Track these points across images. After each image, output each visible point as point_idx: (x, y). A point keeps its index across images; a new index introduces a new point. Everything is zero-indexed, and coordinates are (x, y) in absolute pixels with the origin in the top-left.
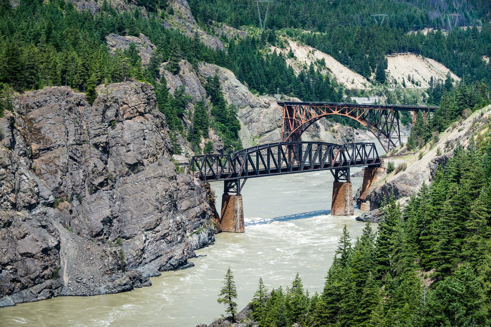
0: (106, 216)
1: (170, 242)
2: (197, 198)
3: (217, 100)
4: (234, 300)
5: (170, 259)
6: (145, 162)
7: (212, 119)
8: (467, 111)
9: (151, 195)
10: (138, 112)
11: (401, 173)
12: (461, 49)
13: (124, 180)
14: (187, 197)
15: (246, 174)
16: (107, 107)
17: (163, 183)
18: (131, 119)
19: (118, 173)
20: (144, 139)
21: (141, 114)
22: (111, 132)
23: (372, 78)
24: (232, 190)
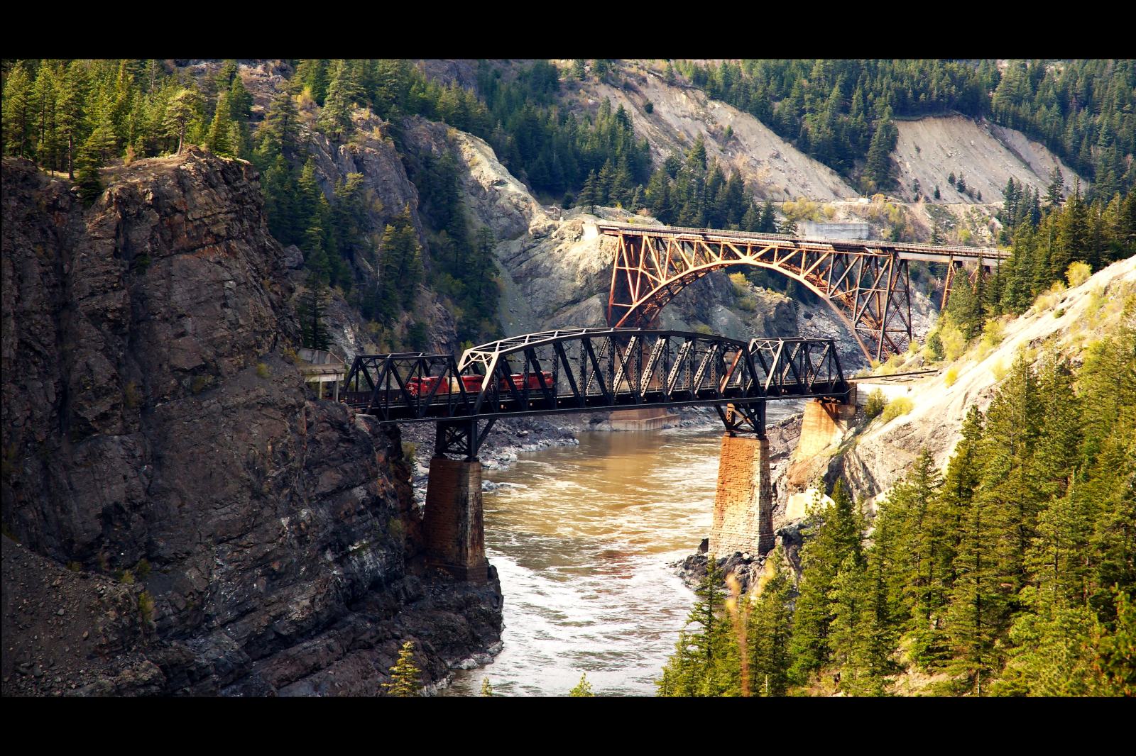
0: (111, 503)
8: (1078, 269)
13: (164, 409)
14: (333, 460)
17: (267, 421)
18: (191, 250)
20: (225, 305)
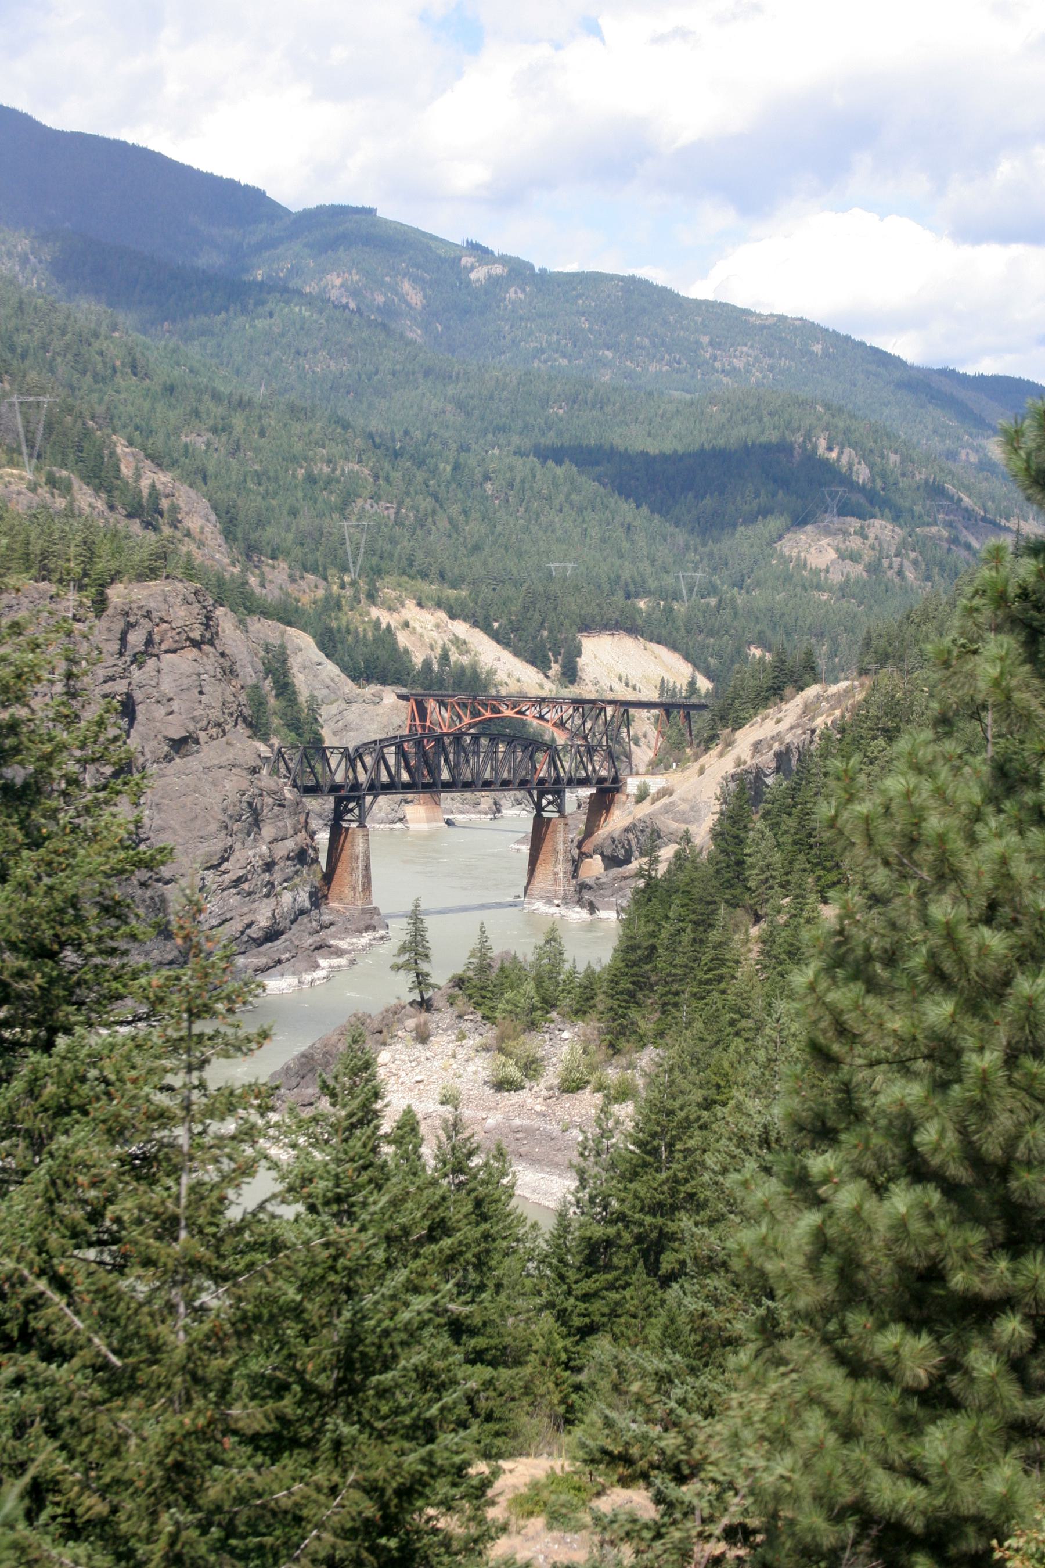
1: (249, 894)
2: (289, 822)
3: (285, 688)
4: (424, 966)
5: (249, 926)
6: (202, 736)
7: (276, 722)
9: (213, 799)
10: (188, 638)
11: (666, 800)
12: (711, 634)
15: (376, 788)
16: (130, 626)
18: (174, 652)
19: (148, 756)
21: (196, 644)
22: (136, 673)
23: (550, 673)
24: (349, 816)
